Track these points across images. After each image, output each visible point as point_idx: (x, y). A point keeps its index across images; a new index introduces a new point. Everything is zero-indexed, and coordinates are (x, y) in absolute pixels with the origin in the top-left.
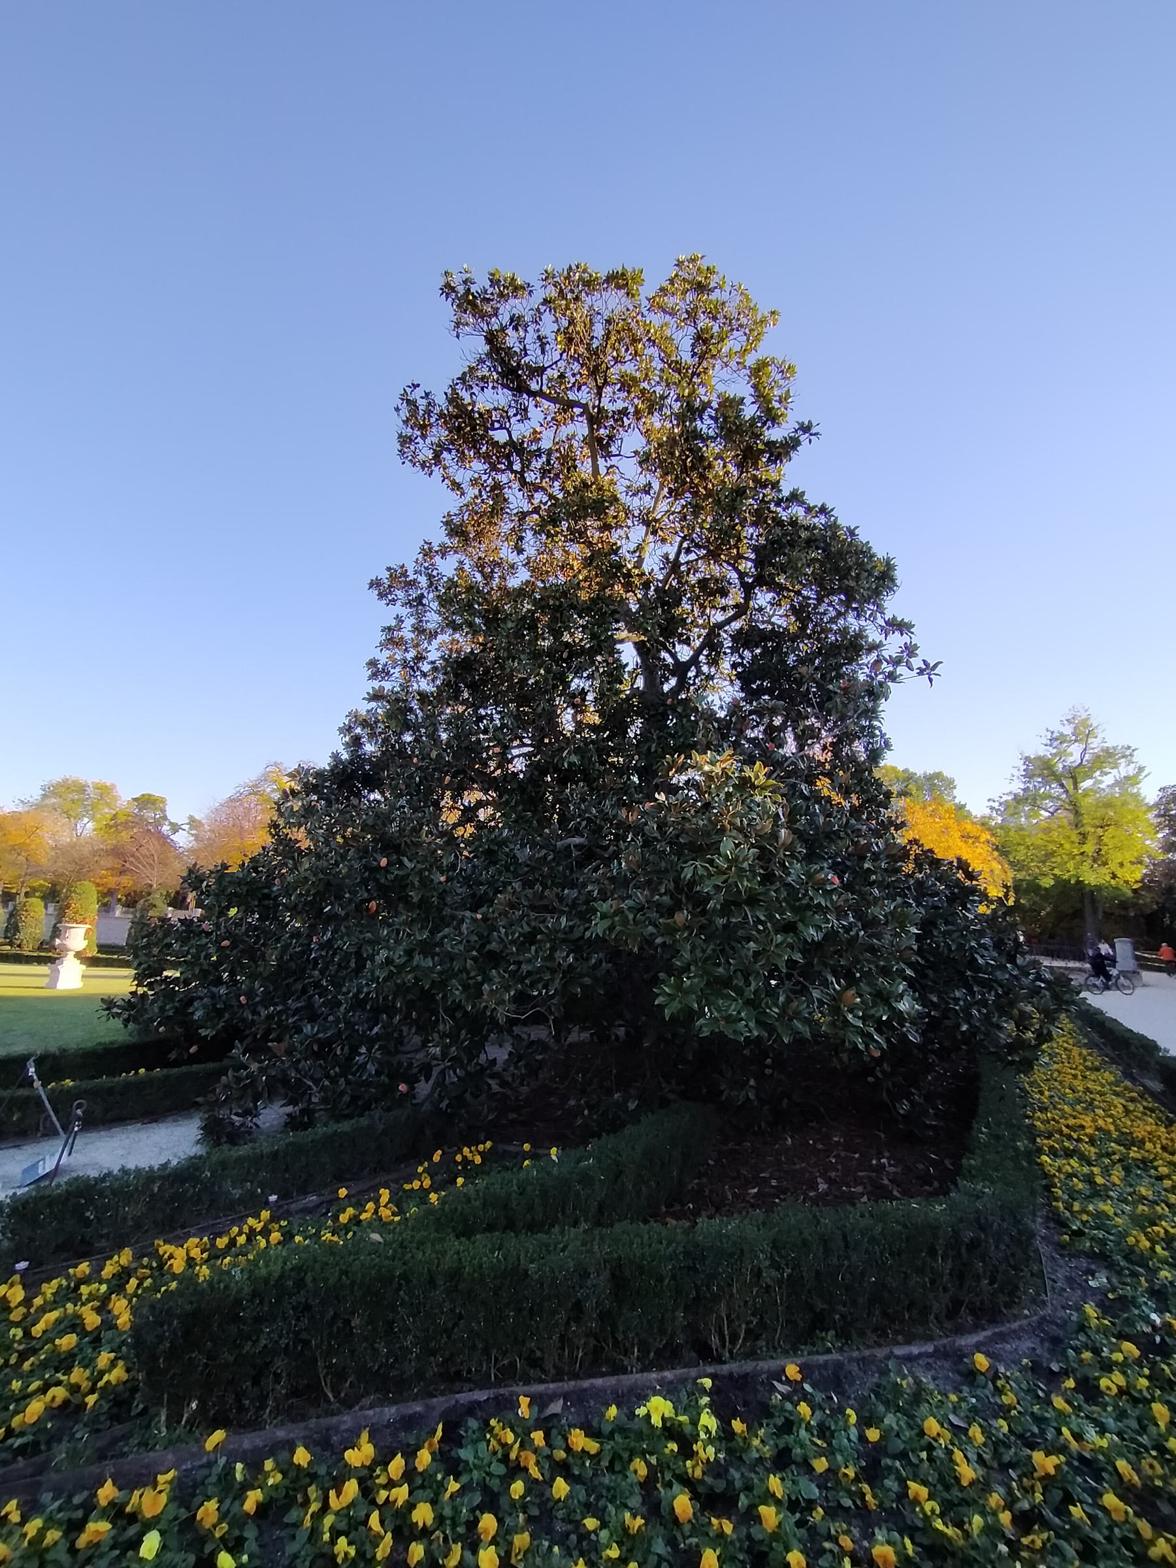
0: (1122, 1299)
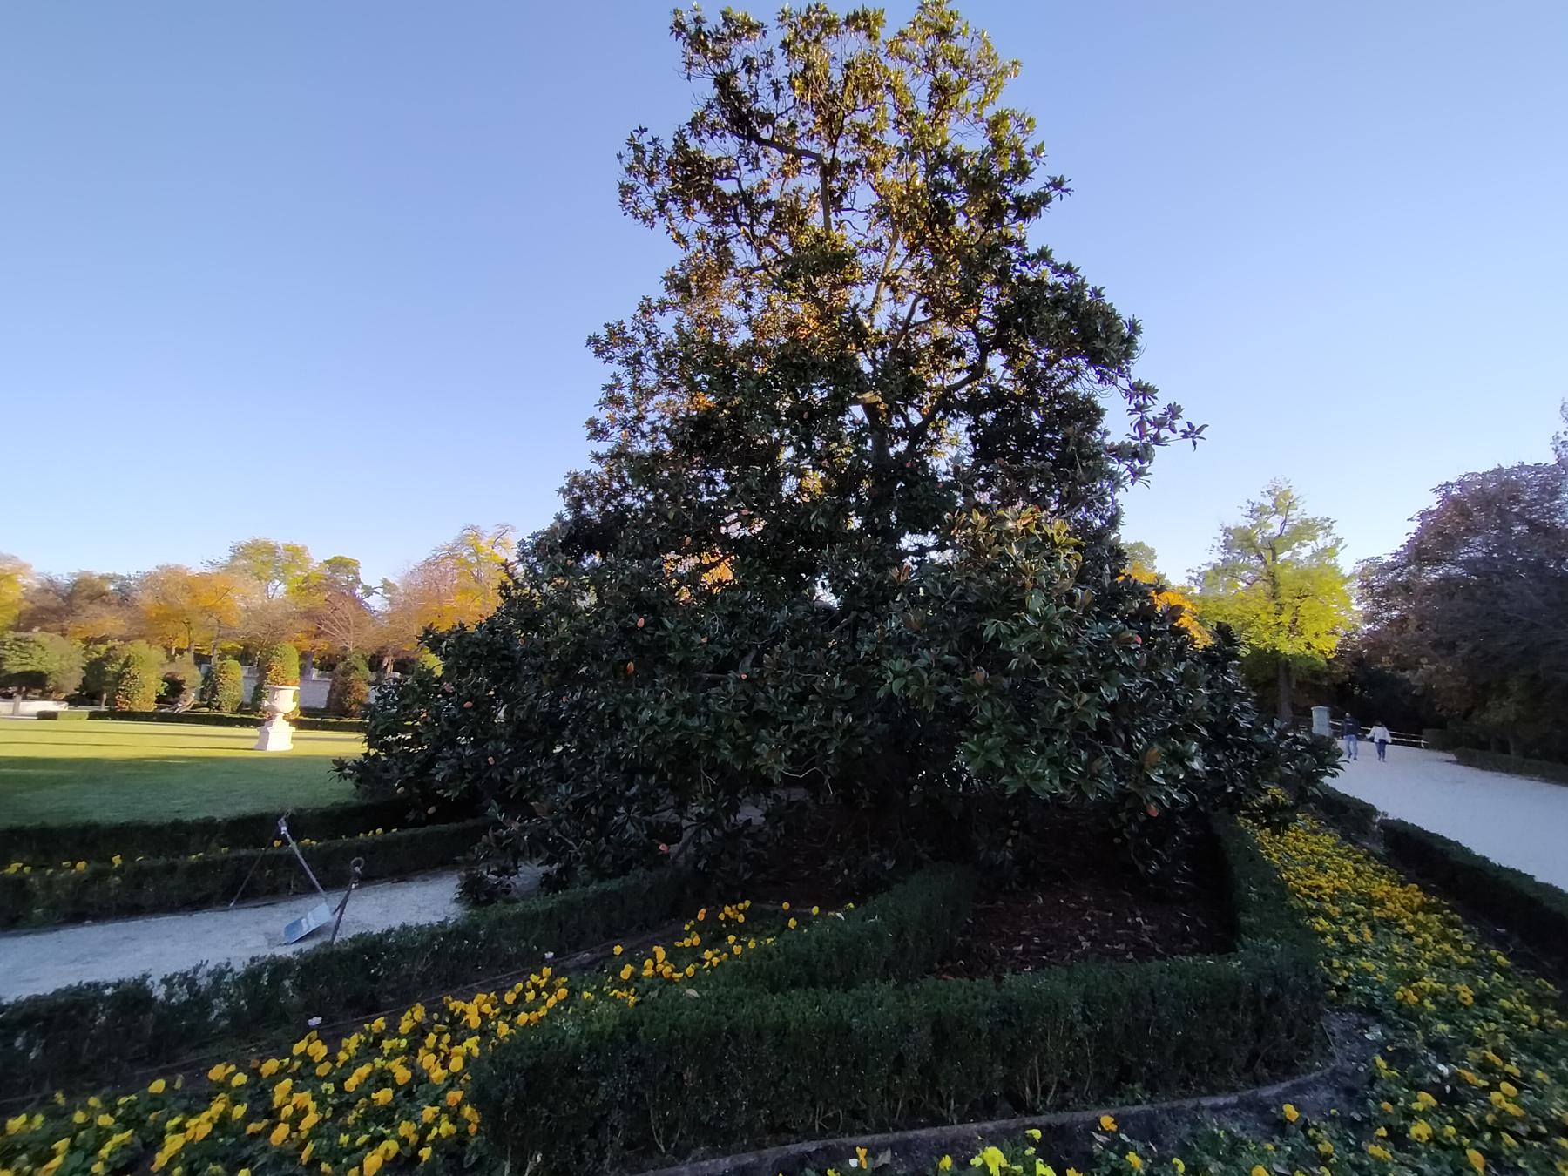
0: (1401, 1051)
